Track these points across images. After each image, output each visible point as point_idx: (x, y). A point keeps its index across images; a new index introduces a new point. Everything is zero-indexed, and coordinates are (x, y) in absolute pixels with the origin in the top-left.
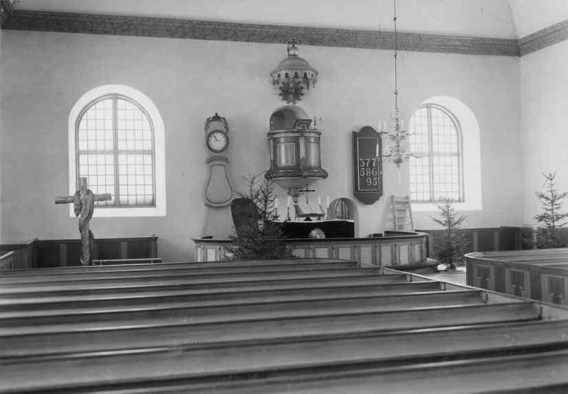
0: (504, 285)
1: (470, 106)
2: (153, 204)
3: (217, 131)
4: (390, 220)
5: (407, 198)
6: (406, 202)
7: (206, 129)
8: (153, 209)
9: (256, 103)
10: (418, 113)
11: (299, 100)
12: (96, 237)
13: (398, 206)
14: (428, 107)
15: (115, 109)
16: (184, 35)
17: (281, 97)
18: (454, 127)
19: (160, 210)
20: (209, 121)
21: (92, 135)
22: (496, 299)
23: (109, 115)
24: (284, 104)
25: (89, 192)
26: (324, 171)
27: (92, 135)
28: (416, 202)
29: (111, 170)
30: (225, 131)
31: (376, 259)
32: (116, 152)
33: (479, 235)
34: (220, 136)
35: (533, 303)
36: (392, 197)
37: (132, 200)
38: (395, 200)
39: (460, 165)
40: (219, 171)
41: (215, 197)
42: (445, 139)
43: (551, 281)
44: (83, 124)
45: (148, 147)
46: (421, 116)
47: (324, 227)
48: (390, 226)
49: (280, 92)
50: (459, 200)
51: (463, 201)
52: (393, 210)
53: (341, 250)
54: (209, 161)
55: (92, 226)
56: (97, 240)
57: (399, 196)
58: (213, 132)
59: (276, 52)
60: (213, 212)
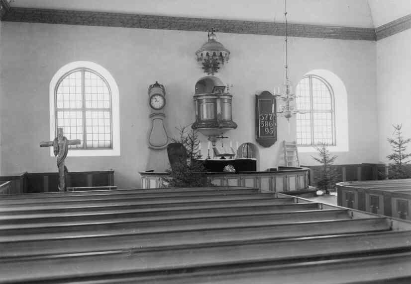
0: (365, 206)
1: (340, 77)
2: (111, 147)
3: (157, 95)
4: (282, 158)
5: (295, 143)
6: (294, 146)
7: (149, 93)
8: (110, 150)
9: (185, 74)
10: (302, 81)
11: (217, 72)
12: (70, 170)
13: (288, 149)
14: (310, 77)
15: (83, 78)
16: (133, 25)
17: (203, 70)
18: (329, 92)
19: (116, 152)
20: (151, 87)
21: (66, 97)
22: (359, 216)
23: (79, 83)
24: (205, 75)
25: (64, 138)
26: (234, 123)
27: (66, 97)
28: (301, 145)
29: (80, 123)
30: (163, 94)
31: (272, 186)
32: (84, 109)
33: (347, 170)
34: (159, 98)
35: (385, 218)
36: (284, 142)
37: (96, 144)
38: (286, 144)
39: (333, 119)
40: (159, 123)
41: (156, 142)
42: (322, 100)
43: (399, 203)
44: (60, 90)
45: (107, 106)
46: (305, 84)
47: (235, 163)
48: (282, 163)
49: (202, 66)
50: (332, 144)
51: (335, 145)
52: (284, 152)
53: (247, 180)
54: (151, 116)
55: (66, 163)
56: (70, 173)
57: (289, 141)
58: (154, 95)
59: (200, 38)
60: (154, 153)
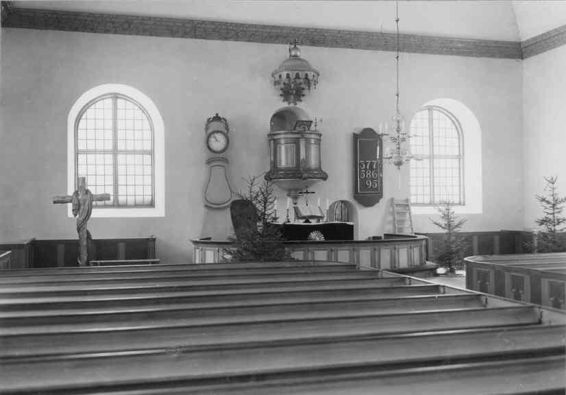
2: (152, 205)
3: (218, 132)
4: (389, 222)
5: (407, 200)
6: (406, 205)
9: (257, 104)
10: (418, 115)
12: (94, 237)
13: (397, 209)
14: (430, 109)
15: (115, 108)
19: (159, 211)
20: (209, 121)
21: (139, 191)
23: (109, 115)
24: (285, 105)
25: (87, 192)
26: (325, 173)
28: (417, 204)
31: (375, 261)
32: (115, 152)
34: (220, 137)
36: (392, 199)
37: (131, 200)
38: (396, 202)
39: (461, 169)
40: (219, 172)
45: (148, 147)
48: (389, 229)
52: (393, 214)
54: (209, 162)
57: (399, 198)
59: (278, 53)
